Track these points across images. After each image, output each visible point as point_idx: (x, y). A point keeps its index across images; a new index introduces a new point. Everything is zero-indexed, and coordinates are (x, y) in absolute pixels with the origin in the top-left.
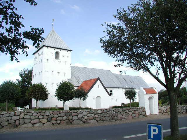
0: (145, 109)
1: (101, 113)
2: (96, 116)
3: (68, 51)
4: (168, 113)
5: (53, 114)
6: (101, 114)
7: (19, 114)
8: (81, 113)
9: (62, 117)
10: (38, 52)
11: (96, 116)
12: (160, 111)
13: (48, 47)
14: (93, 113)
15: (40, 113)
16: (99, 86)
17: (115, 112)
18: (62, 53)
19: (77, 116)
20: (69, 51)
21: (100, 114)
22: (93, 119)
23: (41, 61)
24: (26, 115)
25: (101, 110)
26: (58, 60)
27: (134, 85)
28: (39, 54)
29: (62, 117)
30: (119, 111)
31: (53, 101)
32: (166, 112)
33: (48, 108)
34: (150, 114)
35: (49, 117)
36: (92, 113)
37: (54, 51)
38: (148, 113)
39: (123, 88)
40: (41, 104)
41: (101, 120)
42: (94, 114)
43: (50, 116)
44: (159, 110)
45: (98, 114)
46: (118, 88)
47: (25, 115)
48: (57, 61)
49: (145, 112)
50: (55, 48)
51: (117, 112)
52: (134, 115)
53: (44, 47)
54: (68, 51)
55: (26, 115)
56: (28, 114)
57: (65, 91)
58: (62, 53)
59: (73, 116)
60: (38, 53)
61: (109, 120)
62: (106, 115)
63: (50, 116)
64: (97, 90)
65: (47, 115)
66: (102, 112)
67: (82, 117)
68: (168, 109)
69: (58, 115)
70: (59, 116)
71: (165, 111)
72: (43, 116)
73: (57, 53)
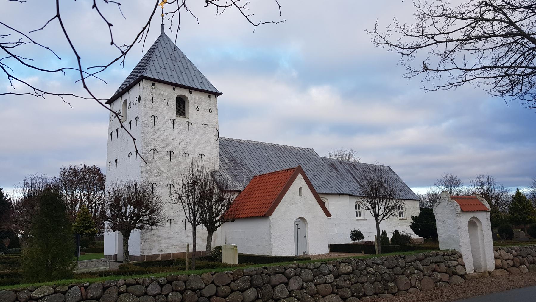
0: (461, 256)
1: (351, 273)
2: (340, 282)
3: (209, 97)
4: (518, 267)
5: (213, 283)
6: (352, 276)
7: (98, 293)
8: (296, 275)
9: (242, 291)
10: (126, 97)
11: (340, 282)
12: (499, 261)
13: (154, 81)
14: (331, 272)
15: (170, 282)
16: (300, 188)
17: (388, 268)
18: (193, 98)
19: (287, 284)
20: (212, 96)
21: (349, 274)
22: (333, 293)
23: (134, 121)
24: (123, 292)
25: (349, 263)
26: (184, 120)
27: (222, 206)
28: (126, 101)
29: (242, 291)
30: (396, 266)
31: (174, 234)
32: (514, 266)
33: (230, 265)
34: (475, 272)
35: (202, 295)
36: (328, 272)
37: (173, 94)
38: (469, 268)
39: (350, 195)
40: (138, 244)
41: (353, 295)
42: (332, 276)
43: (203, 292)
44: (496, 258)
45: (344, 274)
46: (340, 195)
47: (120, 293)
48: (181, 121)
49: (463, 265)
50: (175, 86)
51: (392, 269)
52: (439, 276)
53: (143, 83)
54: (209, 97)
55: (123, 292)
56: (131, 289)
57: (209, 202)
58: (193, 98)
59: (274, 287)
60: (123, 99)
61: (376, 293)
62: (364, 279)
63: (203, 292)
64: (297, 201)
65: (194, 290)
66: (353, 270)
67: (302, 288)
68: (516, 256)
69: (228, 285)
70: (232, 291)
71: (511, 263)
72: (182, 292)
73: (181, 103)
